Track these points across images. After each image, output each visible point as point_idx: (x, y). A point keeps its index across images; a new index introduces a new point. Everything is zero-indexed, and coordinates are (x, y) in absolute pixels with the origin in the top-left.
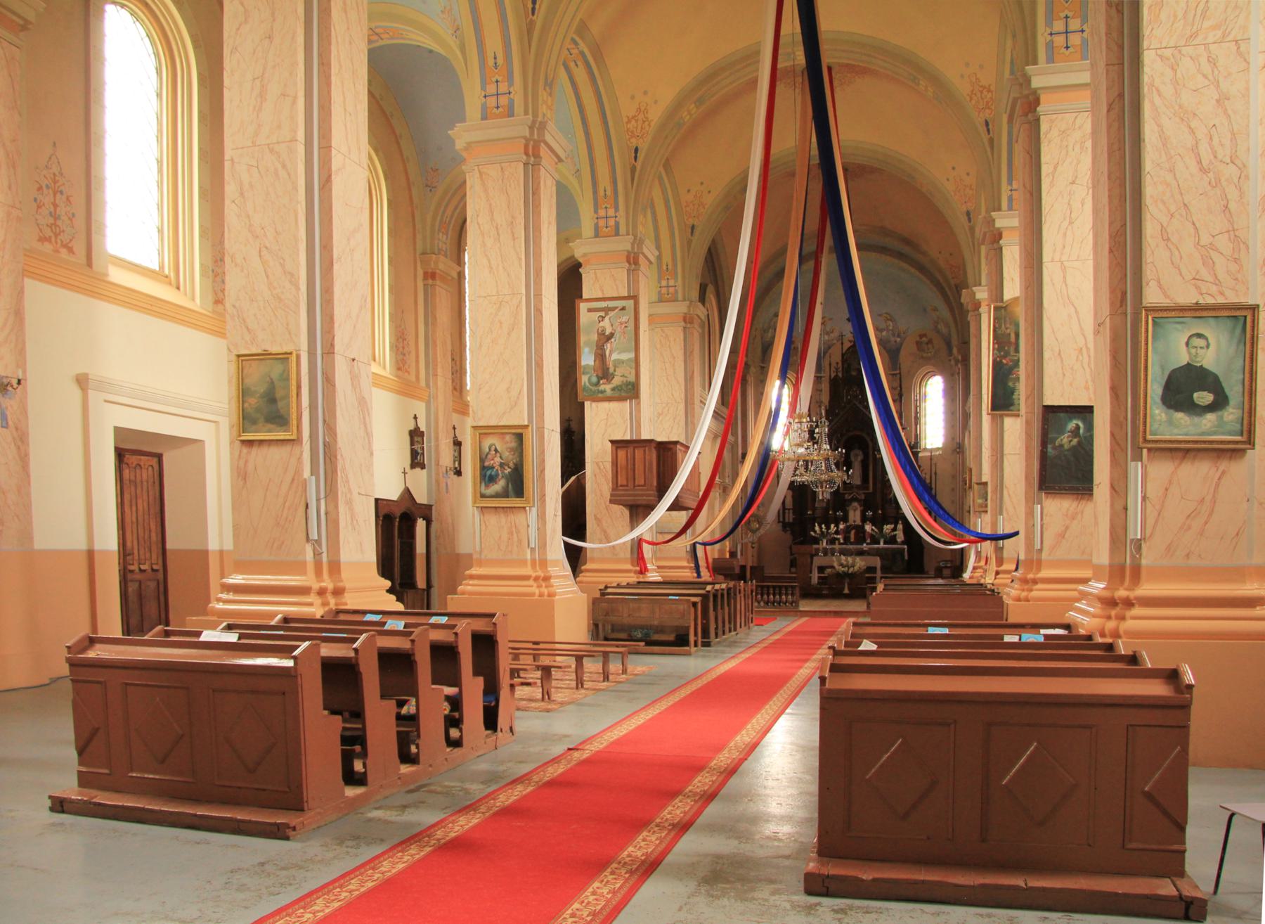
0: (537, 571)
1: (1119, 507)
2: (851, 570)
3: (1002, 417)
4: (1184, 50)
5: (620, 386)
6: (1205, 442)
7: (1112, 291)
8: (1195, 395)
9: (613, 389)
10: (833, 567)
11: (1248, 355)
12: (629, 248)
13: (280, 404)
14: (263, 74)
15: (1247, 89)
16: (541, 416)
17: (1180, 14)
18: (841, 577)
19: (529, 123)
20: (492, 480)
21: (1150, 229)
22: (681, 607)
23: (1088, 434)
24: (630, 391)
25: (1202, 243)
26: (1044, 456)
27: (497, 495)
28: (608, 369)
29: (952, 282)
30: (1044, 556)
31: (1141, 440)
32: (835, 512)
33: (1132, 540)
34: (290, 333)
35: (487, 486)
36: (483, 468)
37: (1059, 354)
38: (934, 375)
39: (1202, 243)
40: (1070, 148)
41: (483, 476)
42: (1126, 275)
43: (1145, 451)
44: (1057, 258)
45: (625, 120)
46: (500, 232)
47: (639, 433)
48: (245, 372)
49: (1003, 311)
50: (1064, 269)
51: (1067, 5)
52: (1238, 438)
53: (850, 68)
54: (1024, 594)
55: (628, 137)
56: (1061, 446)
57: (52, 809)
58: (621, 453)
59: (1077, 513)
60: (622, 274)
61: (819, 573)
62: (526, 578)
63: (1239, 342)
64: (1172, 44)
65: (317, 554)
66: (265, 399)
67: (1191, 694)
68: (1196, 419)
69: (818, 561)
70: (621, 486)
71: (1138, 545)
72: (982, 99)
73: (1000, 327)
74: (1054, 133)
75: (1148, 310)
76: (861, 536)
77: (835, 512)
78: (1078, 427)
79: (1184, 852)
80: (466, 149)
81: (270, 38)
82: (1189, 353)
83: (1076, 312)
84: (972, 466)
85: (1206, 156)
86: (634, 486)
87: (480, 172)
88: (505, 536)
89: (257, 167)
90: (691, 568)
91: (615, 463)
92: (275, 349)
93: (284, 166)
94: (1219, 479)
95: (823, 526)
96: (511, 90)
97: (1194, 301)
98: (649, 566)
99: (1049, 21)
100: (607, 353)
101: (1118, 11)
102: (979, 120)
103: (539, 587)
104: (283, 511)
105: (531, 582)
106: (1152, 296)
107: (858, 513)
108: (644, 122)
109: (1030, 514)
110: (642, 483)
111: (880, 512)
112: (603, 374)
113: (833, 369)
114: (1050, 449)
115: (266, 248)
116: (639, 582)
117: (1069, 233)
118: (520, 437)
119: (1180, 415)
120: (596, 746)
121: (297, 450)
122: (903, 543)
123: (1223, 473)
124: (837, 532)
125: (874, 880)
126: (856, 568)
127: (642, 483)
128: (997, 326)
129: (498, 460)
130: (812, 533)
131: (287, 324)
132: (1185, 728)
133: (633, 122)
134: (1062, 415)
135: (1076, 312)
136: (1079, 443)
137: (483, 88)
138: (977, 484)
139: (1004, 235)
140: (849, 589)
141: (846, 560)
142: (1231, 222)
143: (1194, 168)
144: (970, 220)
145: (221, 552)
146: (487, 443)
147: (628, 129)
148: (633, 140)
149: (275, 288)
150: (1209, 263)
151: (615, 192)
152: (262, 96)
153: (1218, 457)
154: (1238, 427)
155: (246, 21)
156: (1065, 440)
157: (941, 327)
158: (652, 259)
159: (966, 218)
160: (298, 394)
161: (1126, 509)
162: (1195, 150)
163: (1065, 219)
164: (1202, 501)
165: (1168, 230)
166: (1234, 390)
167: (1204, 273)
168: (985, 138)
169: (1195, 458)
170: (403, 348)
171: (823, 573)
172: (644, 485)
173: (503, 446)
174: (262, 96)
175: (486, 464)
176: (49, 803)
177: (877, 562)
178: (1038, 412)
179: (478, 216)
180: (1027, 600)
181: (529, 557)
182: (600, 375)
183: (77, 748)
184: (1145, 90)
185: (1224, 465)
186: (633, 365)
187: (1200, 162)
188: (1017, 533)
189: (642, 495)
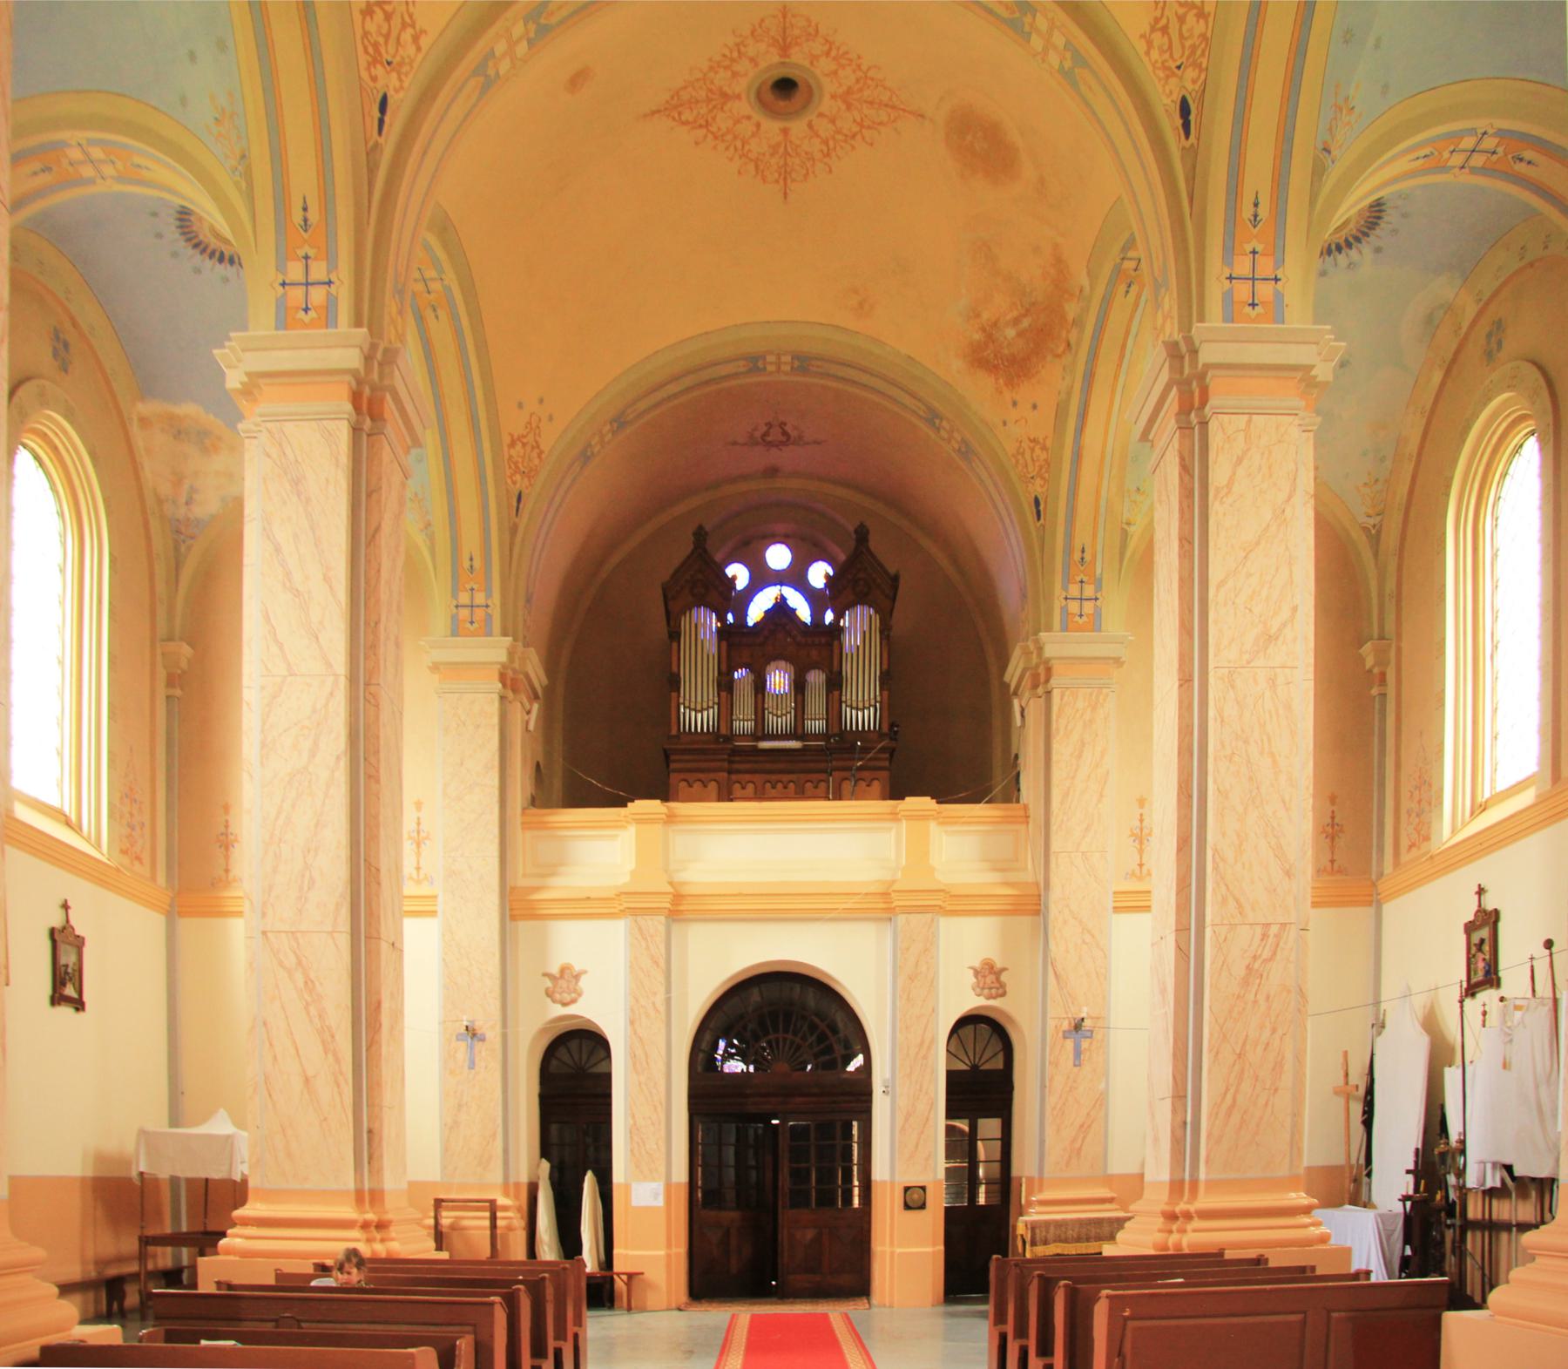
0: (364, 1212)
51: (1082, 568)
99: (1068, 580)
103: (369, 1241)
133: (519, 446)
140: (806, 1067)
147: (510, 457)
170: (131, 815)
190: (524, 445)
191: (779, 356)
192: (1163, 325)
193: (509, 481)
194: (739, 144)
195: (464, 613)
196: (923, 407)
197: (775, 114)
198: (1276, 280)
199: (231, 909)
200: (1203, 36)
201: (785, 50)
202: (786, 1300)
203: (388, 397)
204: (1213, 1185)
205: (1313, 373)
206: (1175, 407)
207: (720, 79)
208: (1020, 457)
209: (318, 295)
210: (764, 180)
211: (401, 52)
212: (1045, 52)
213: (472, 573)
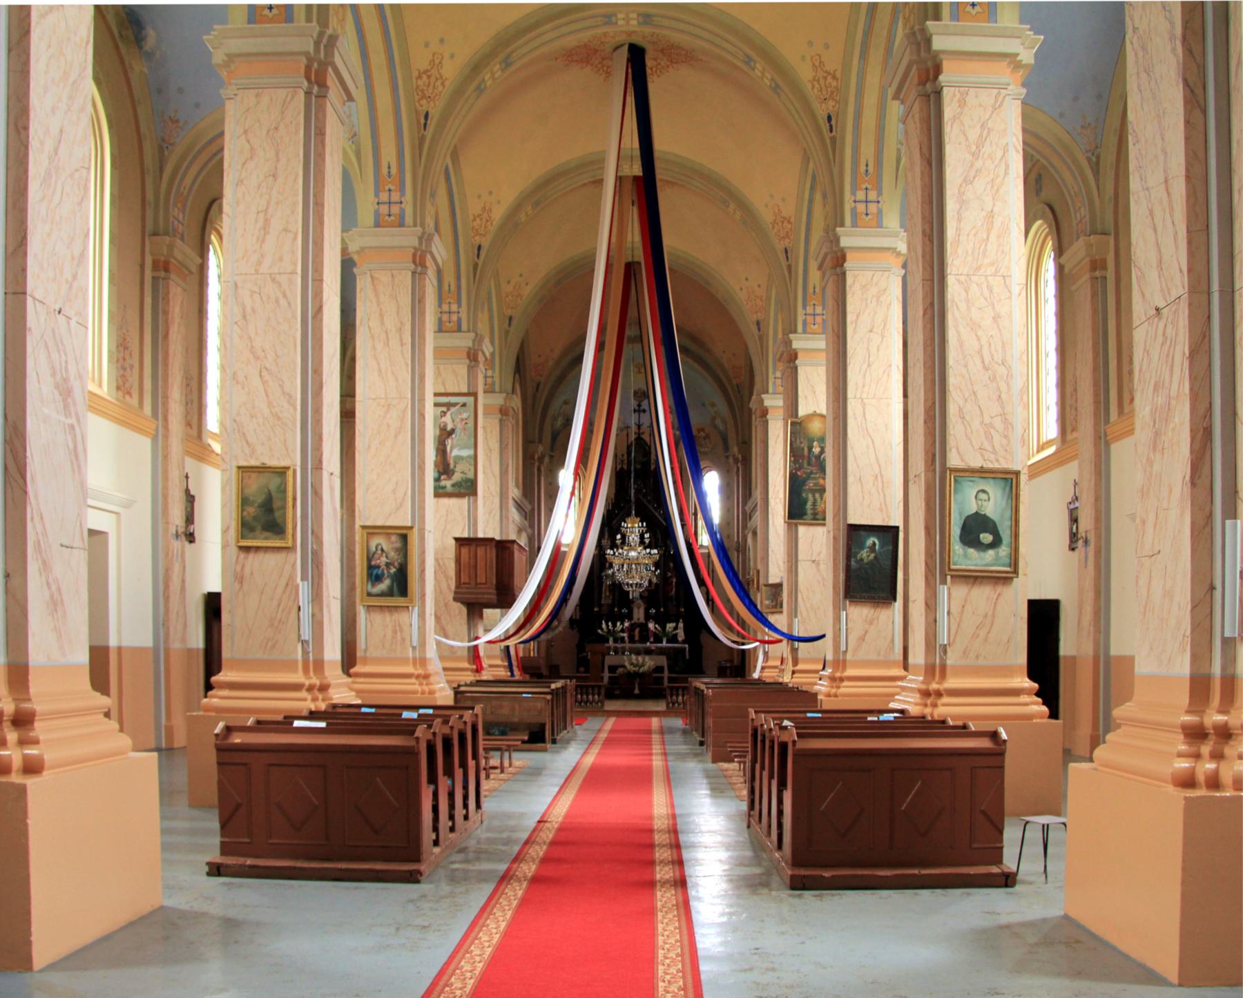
1: (931, 619)
2: (642, 670)
3: (796, 525)
4: (973, 278)
5: (460, 483)
6: (987, 571)
7: (926, 453)
8: (981, 536)
9: (453, 486)
10: (624, 666)
11: (1014, 508)
12: (470, 345)
13: (277, 514)
14: (267, 208)
15: (1011, 312)
16: (422, 518)
17: (970, 251)
18: (632, 676)
19: (419, 234)
21: (952, 409)
23: (645, 459)
24: (468, 489)
25: (985, 422)
26: (848, 568)
27: (382, 594)
28: (448, 465)
29: (734, 382)
30: (849, 657)
31: (947, 569)
32: (620, 609)
33: (940, 645)
34: (287, 450)
35: (373, 585)
37: (860, 479)
38: (711, 470)
39: (985, 422)
40: (869, 301)
41: (370, 575)
42: (935, 441)
43: (949, 577)
44: (858, 396)
45: (471, 218)
46: (390, 337)
47: (476, 531)
48: (245, 481)
49: (798, 426)
50: (864, 405)
51: (867, 179)
52: (1008, 569)
53: (667, 182)
54: (834, 691)
55: (472, 235)
56: (862, 560)
57: (209, 874)
58: (465, 551)
59: (873, 619)
60: (463, 370)
61: (610, 672)
63: (1009, 497)
64: (965, 273)
65: (305, 653)
66: (263, 509)
67: (1005, 745)
68: (982, 554)
69: (611, 660)
70: (464, 584)
71: (944, 649)
72: (783, 228)
73: (796, 439)
75: (951, 470)
76: (645, 635)
77: (620, 609)
78: (874, 544)
79: (1002, 848)
80: (358, 252)
81: (274, 176)
82: (977, 504)
83: (873, 443)
84: (759, 567)
85: (987, 359)
86: (477, 584)
87: (372, 277)
89: (260, 294)
90: (504, 666)
91: (458, 560)
93: (285, 296)
94: (997, 599)
95: (610, 624)
96: (403, 200)
97: (980, 465)
98: (485, 665)
100: (448, 448)
101: (930, 240)
102: (780, 246)
103: (421, 684)
104: (277, 613)
106: (954, 461)
107: (642, 611)
108: (487, 221)
109: (837, 619)
110: (484, 581)
111: (662, 610)
112: (444, 469)
113: (618, 461)
114: (853, 563)
115: (267, 369)
116: (478, 681)
117: (868, 374)
118: (404, 538)
119: (971, 551)
121: (291, 556)
122: (684, 642)
123: (999, 595)
124: (622, 630)
125: (833, 877)
126: (646, 668)
127: (484, 581)
128: (793, 439)
129: (384, 559)
130: (599, 631)
131: (285, 441)
132: (1002, 767)
134: (863, 533)
135: (873, 443)
136: (876, 558)
137: (377, 195)
138: (766, 585)
139: (800, 355)
140: (639, 689)
141: (637, 660)
142: (1003, 408)
144: (759, 329)
145: (120, 649)
146: (375, 542)
147: (417, 87)
148: (477, 238)
149: (274, 407)
150: (989, 437)
152: (266, 228)
153: (996, 583)
154: (1008, 561)
155: (252, 158)
156: (865, 555)
157: (718, 422)
158: (488, 354)
159: (756, 327)
160: (294, 506)
161: (936, 621)
162: (980, 352)
163: (864, 362)
164: (986, 616)
165: (964, 411)
166: (1006, 535)
167: (986, 445)
168: (784, 263)
169: (981, 583)
171: (615, 673)
172: (486, 583)
173: (388, 545)
174: (266, 228)
175: (373, 563)
176: (206, 869)
177: (663, 661)
178: (842, 528)
179: (369, 319)
180: (836, 696)
181: (411, 655)
182: (441, 471)
183: (220, 822)
184: (949, 304)
185: (999, 589)
186: (473, 462)
187: (983, 362)
188: (823, 636)
189: (483, 594)
190: (429, 77)
192: (909, 16)
193: (417, 104)
194: (605, 68)
196: (741, 53)
198: (878, 202)
199: (212, 460)
200: (836, 88)
202: (614, 477)
203: (330, 69)
205: (1019, 58)
206: (916, 81)
208: (815, 83)
211: (435, 91)
213: (389, 177)
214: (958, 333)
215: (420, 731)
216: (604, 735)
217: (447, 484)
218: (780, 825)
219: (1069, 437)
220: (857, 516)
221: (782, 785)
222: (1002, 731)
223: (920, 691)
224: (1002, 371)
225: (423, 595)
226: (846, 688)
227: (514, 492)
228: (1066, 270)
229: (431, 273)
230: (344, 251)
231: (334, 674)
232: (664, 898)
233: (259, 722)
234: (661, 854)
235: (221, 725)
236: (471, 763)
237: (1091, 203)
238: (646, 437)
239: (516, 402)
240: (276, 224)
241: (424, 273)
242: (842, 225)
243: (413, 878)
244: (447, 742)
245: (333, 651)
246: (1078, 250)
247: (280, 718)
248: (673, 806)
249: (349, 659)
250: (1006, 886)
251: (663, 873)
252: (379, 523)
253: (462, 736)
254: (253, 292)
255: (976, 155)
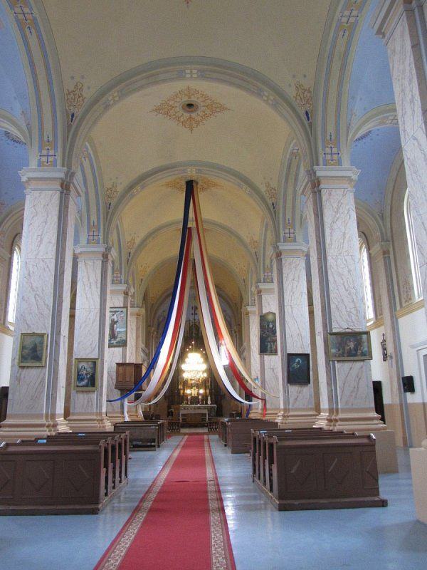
13: (38, 353)
20: (82, 380)
21: (333, 306)
22: (153, 431)
24: (123, 344)
27: (84, 386)
36: (78, 375)
41: (78, 379)
47: (125, 360)
58: (121, 368)
60: (121, 298)
62: (94, 420)
74: (287, 264)
79: (378, 488)
88: (86, 402)
92: (39, 332)
105: (95, 422)
114: (290, 369)
120: (160, 483)
121: (44, 370)
129: (85, 372)
143: (344, 290)
150: (350, 316)
151: (121, 268)
160: (47, 349)
173: (88, 366)
174: (41, 241)
191: (191, 77)
195: (44, 159)
197: (188, 112)
201: (190, 97)
204: (344, 411)
207: (172, 103)
209: (51, 159)
210: (185, 127)
212: (268, 100)
214: (334, 277)
215: (102, 443)
216: (182, 443)
217: (114, 342)
218: (271, 481)
219: (379, 317)
220: (292, 349)
221: (271, 462)
222: (372, 434)
223: (327, 420)
224: (353, 291)
225: (102, 386)
226: (290, 420)
227: (142, 345)
228: (372, 255)
229: (110, 262)
230: (74, 254)
231: (60, 420)
232: (214, 518)
233: (23, 441)
234: (211, 496)
235: (4, 443)
236: (124, 457)
237: (381, 230)
238: (197, 324)
239: (143, 311)
240: (46, 240)
241: (107, 261)
242: (280, 242)
243: (95, 512)
244: (113, 448)
245: (60, 409)
246: (377, 248)
247: (33, 439)
248: (216, 474)
249: (67, 414)
250: (383, 506)
251: (213, 505)
252: (84, 357)
253: (120, 445)
254: (34, 266)
255: (337, 212)
